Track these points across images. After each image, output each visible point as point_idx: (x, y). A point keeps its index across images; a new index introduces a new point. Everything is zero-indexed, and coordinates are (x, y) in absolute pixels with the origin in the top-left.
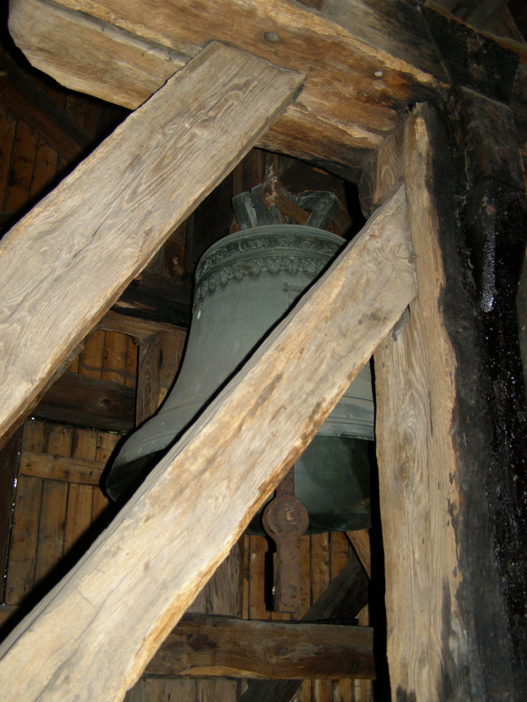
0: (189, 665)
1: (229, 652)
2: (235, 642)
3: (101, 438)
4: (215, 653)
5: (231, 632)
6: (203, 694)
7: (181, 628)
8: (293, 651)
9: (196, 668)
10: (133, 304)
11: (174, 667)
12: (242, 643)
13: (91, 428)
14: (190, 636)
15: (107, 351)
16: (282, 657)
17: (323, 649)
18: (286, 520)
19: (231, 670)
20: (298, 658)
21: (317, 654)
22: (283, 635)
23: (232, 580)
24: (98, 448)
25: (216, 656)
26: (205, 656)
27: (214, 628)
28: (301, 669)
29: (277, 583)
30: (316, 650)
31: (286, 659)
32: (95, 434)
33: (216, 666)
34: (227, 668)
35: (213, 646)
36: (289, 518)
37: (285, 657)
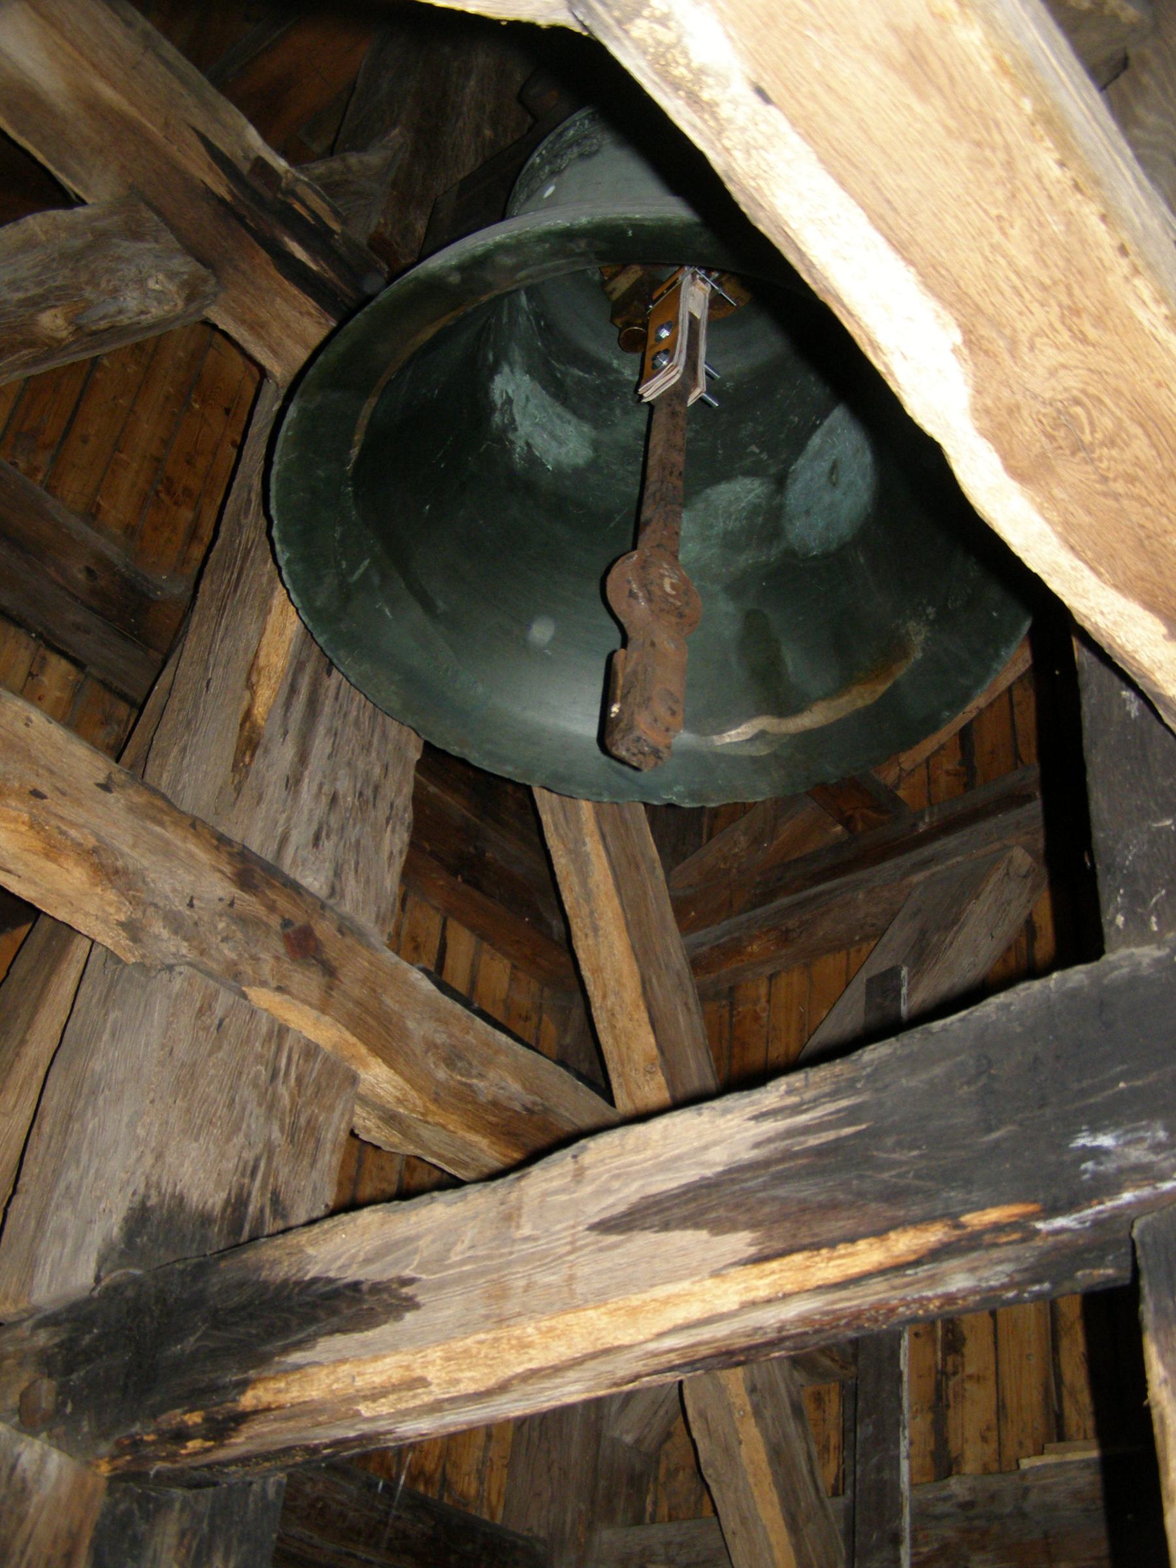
0: (274, 984)
1: (358, 1003)
2: (374, 991)
3: (44, 658)
4: (331, 989)
5: (371, 963)
6: (289, 1058)
7: (275, 897)
8: (481, 1076)
9: (287, 997)
10: (316, 262)
11: (241, 968)
12: (388, 1001)
13: (29, 630)
14: (286, 923)
15: (99, 505)
16: (459, 1078)
17: (540, 1107)
18: (661, 587)
19: (354, 1045)
20: (490, 1098)
21: (527, 1109)
22: (468, 1033)
23: (389, 866)
24: (30, 674)
25: (331, 996)
26: (307, 980)
27: (340, 936)
28: (490, 1123)
29: (625, 697)
30: (529, 1099)
31: (465, 1084)
32: (33, 645)
33: (327, 1018)
34: (348, 1036)
35: (330, 971)
36: (668, 589)
37: (464, 1079)
